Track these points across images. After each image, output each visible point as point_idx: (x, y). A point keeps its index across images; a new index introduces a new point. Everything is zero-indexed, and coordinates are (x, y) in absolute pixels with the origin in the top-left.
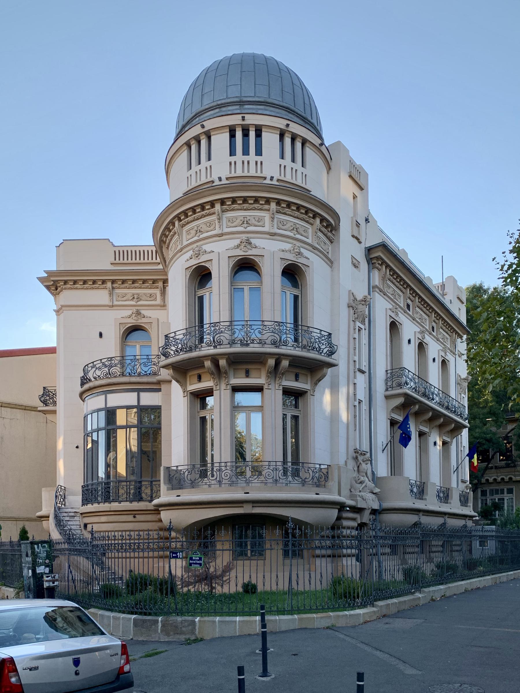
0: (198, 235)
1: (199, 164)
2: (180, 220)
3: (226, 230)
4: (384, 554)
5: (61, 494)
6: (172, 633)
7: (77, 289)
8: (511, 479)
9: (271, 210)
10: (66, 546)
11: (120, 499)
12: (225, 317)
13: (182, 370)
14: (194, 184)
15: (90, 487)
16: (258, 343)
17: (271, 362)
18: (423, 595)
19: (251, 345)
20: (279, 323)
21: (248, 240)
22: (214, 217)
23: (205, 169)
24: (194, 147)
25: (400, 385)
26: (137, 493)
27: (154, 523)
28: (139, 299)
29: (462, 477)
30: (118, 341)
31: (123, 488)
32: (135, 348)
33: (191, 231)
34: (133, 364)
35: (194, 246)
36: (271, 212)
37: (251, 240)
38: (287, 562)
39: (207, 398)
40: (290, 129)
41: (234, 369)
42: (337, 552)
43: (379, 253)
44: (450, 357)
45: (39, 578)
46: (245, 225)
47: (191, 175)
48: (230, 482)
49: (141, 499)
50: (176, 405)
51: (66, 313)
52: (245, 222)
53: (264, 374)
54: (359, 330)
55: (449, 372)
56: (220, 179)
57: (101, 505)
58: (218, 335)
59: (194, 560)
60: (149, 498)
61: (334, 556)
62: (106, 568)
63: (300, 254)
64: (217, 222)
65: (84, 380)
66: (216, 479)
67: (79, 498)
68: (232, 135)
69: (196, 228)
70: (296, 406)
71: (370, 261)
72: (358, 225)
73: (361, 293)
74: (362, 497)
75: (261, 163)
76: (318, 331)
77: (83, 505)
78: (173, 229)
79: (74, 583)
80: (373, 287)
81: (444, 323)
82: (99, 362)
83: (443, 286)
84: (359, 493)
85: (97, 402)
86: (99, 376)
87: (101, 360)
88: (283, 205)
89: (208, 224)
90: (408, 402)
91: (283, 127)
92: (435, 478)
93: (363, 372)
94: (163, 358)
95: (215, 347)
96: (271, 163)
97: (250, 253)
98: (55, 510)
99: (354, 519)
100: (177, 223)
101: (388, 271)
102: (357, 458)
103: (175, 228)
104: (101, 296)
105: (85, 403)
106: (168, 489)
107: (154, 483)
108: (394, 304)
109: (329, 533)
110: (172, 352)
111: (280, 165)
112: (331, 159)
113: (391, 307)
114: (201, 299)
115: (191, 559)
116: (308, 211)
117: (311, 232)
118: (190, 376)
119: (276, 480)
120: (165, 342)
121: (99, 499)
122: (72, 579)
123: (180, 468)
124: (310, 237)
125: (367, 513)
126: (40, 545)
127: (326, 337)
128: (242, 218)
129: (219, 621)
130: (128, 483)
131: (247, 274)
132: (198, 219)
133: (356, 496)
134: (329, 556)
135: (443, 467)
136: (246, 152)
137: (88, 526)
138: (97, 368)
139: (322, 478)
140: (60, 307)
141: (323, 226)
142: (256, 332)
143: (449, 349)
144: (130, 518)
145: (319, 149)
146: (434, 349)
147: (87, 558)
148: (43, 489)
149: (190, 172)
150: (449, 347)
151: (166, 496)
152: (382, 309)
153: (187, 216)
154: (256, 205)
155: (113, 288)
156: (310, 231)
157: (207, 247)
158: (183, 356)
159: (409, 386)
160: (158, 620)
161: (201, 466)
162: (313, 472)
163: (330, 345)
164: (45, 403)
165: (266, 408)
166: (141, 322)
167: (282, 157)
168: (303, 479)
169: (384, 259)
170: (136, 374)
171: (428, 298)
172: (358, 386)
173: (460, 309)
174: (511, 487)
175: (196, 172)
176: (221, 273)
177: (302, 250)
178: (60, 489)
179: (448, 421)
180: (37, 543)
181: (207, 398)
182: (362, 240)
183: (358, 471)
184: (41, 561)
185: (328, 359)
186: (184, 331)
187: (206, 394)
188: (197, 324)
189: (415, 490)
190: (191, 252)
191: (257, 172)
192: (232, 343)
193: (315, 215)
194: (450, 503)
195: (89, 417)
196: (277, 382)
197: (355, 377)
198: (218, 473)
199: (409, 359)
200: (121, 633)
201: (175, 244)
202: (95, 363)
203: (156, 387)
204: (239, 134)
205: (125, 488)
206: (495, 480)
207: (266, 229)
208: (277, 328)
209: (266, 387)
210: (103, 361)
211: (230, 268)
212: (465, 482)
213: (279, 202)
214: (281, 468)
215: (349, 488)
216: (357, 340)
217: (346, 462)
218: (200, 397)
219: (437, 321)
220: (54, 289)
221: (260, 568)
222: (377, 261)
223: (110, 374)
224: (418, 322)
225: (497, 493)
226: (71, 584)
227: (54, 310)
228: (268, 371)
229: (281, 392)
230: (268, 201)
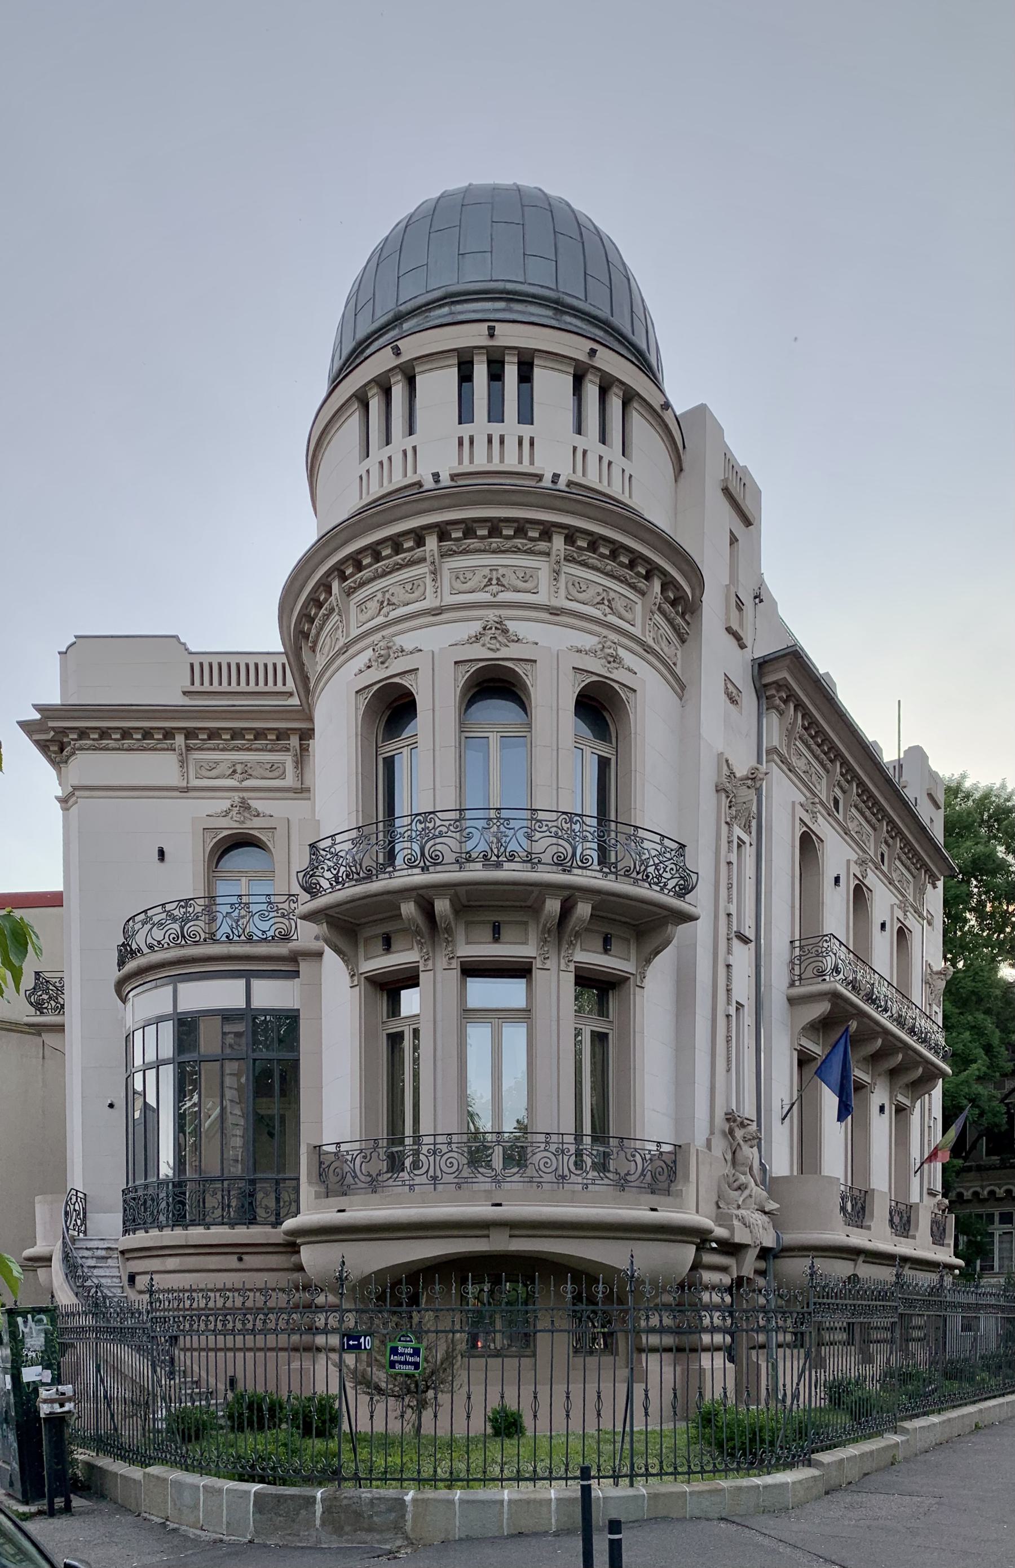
0: (385, 610)
1: (388, 442)
2: (344, 578)
3: (450, 599)
4: (831, 1344)
5: (77, 1208)
6: (347, 1529)
7: (108, 749)
9: (554, 552)
10: (88, 1321)
11: (208, 1219)
12: (448, 800)
13: (352, 926)
14: (376, 491)
15: (140, 1193)
16: (524, 862)
17: (553, 906)
18: (904, 1438)
19: (507, 865)
21: (500, 623)
22: (423, 569)
23: (401, 455)
24: (375, 404)
26: (246, 1205)
28: (247, 774)
29: (929, 1183)
30: (201, 868)
32: (242, 880)
33: (369, 604)
34: (236, 914)
35: (376, 637)
36: (553, 558)
37: (506, 622)
39: (402, 992)
40: (597, 362)
42: (687, 1340)
43: (782, 674)
44: (911, 922)
45: (28, 1395)
46: (495, 588)
47: (368, 471)
48: (456, 1180)
49: (252, 1221)
50: (333, 1007)
51: (83, 804)
52: (494, 582)
53: (533, 936)
54: (739, 846)
55: (907, 958)
57: (167, 1232)
58: (431, 843)
59: (402, 1354)
60: (273, 1219)
61: (680, 1350)
62: (179, 1371)
63: (616, 659)
64: (428, 580)
65: (126, 953)
66: (427, 1172)
67: (117, 1219)
68: (466, 377)
70: (602, 1010)
71: (761, 690)
72: (740, 605)
74: (742, 1220)
76: (657, 838)
77: (126, 1232)
78: (326, 600)
79: (109, 1406)
80: (768, 752)
81: (905, 845)
82: (159, 909)
84: (736, 1212)
85: (154, 1001)
86: (159, 942)
88: (580, 543)
89: (408, 587)
91: (583, 357)
94: (305, 896)
95: (425, 869)
96: (554, 442)
98: (64, 1244)
99: (724, 1269)
100: (335, 586)
102: (731, 1132)
103: (332, 598)
104: (160, 766)
105: (129, 1004)
106: (318, 1196)
108: (808, 795)
110: (325, 884)
111: (575, 449)
112: (684, 447)
113: (803, 799)
114: (389, 764)
115: (394, 1351)
116: (635, 559)
117: (640, 613)
118: (366, 940)
119: (563, 1177)
120: (311, 859)
121: (162, 1218)
122: (105, 1397)
123: (344, 1147)
124: (638, 622)
126: (29, 1316)
127: (673, 853)
128: (486, 571)
130: (226, 1183)
131: (497, 711)
132: (384, 574)
134: (668, 1350)
135: (896, 1156)
136: (496, 414)
137: (138, 1278)
138: (154, 925)
139: (666, 1173)
140: (71, 789)
142: (520, 834)
143: (912, 906)
144: (232, 1262)
146: (883, 902)
147: (139, 1349)
148: (38, 1198)
149: (368, 463)
151: (313, 1211)
152: (783, 800)
154: (519, 542)
155: (188, 749)
156: (638, 608)
157: (407, 641)
159: (841, 976)
160: (314, 1498)
161: (394, 1144)
162: (644, 1159)
164: (39, 1007)
165: (540, 1014)
166: (253, 825)
167: (579, 431)
168: (622, 1175)
170: (243, 938)
172: (735, 970)
174: (1006, 1209)
175: (381, 463)
176: (437, 700)
177: (622, 652)
178: (74, 1200)
179: (915, 1059)
180: (24, 1314)
181: (402, 992)
182: (748, 641)
183: (734, 1162)
186: (354, 834)
187: (398, 981)
188: (381, 818)
191: (520, 462)
192: (465, 859)
193: (652, 571)
195: (138, 1034)
196: (563, 954)
197: (729, 951)
198: (431, 1159)
199: (835, 915)
200: (224, 1527)
201: (330, 637)
203: (288, 966)
204: (480, 371)
205: (219, 1193)
206: (976, 1194)
207: (541, 598)
208: (565, 826)
209: (538, 964)
210: (168, 907)
211: (459, 690)
212: (935, 1195)
213: (571, 535)
215: (715, 1199)
217: (709, 1142)
219: (890, 841)
220: (56, 748)
221: (527, 1375)
222: (778, 691)
223: (183, 936)
226: (102, 1406)
227: (57, 798)
228: (545, 925)
229: (571, 977)
230: (547, 531)
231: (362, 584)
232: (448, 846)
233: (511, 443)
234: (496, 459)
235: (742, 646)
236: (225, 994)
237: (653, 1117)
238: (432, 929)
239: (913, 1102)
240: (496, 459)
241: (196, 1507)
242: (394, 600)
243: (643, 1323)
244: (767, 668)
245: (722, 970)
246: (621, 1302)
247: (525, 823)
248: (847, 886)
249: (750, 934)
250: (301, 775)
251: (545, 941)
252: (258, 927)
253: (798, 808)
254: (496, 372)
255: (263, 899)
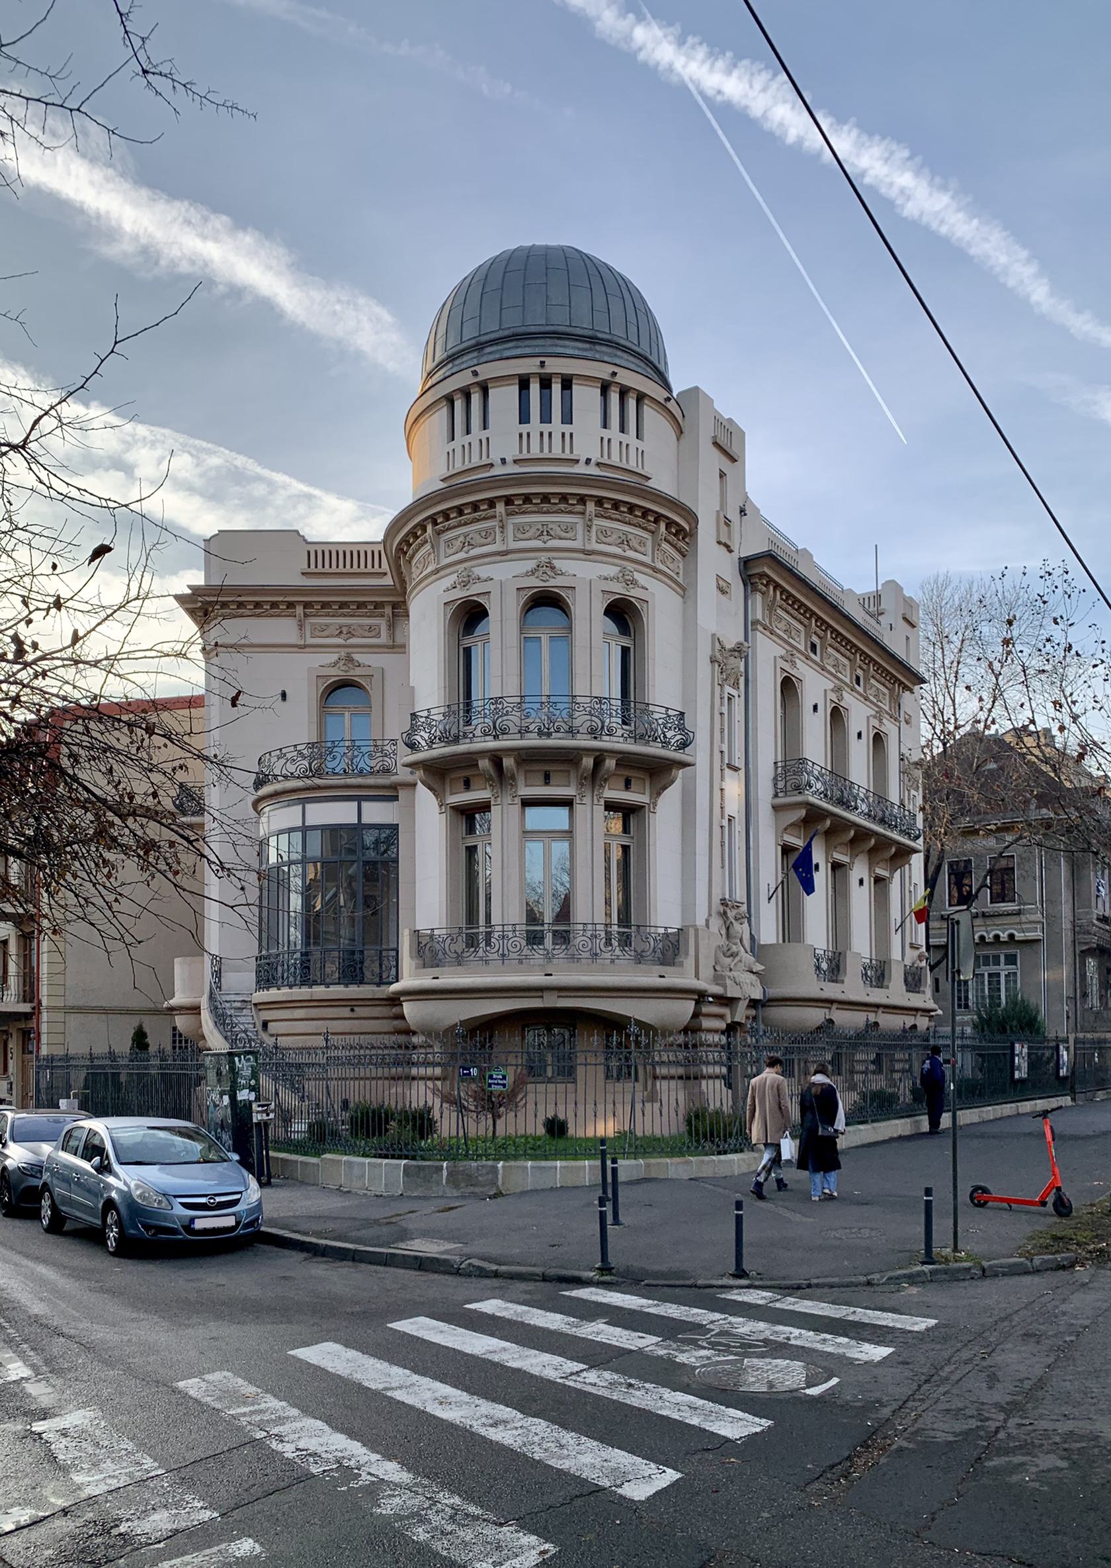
2: (435, 523)
6: (463, 1185)
8: (1011, 936)
12: (512, 689)
13: (440, 773)
17: (588, 762)
20: (600, 700)
24: (459, 404)
25: (798, 789)
27: (385, 1021)
31: (333, 963)
35: (461, 567)
37: (554, 562)
38: (610, 1087)
40: (617, 379)
41: (526, 772)
42: (693, 1070)
44: (889, 727)
49: (362, 982)
54: (729, 699)
56: (503, 461)
57: (295, 990)
60: (377, 980)
61: (688, 1078)
63: (634, 582)
67: (249, 978)
69: (462, 539)
72: (728, 522)
73: (733, 636)
75: (571, 435)
76: (663, 710)
83: (878, 597)
84: (729, 974)
87: (295, 746)
89: (483, 534)
90: (812, 817)
91: (607, 377)
92: (861, 945)
93: (736, 769)
95: (496, 737)
96: (587, 437)
97: (552, 583)
99: (721, 1017)
100: (429, 528)
101: (778, 593)
102: (725, 913)
104: (282, 629)
107: (384, 953)
109: (681, 1039)
114: (468, 652)
115: (491, 1077)
119: (596, 954)
123: (436, 932)
125: (743, 1005)
129: (532, 1167)
132: (466, 524)
133: (723, 977)
134: (680, 1078)
136: (546, 418)
139: (671, 949)
141: (670, 533)
144: (346, 1012)
145: (662, 406)
146: (859, 716)
150: (887, 708)
151: (410, 977)
153: (447, 518)
154: (562, 506)
155: (306, 615)
157: (482, 571)
158: (441, 750)
162: (655, 940)
163: (681, 728)
166: (354, 673)
169: (772, 576)
171: (848, 631)
172: (726, 793)
173: (908, 638)
174: (1012, 951)
177: (637, 575)
182: (735, 547)
184: (243, 1082)
185: (678, 756)
189: (824, 966)
190: (454, 577)
191: (563, 451)
192: (523, 732)
194: (887, 987)
197: (722, 779)
199: (815, 745)
202: (284, 751)
203: (390, 793)
204: (535, 387)
208: (597, 706)
210: (299, 748)
214: (603, 934)
216: (726, 716)
217: (707, 921)
218: (468, 816)
219: (865, 667)
221: (571, 1097)
224: (831, 674)
225: (986, 964)
231: (449, 529)
232: (513, 720)
233: (557, 438)
234: (546, 449)
235: (731, 551)
236: (342, 813)
237: (664, 912)
238: (501, 777)
239: (892, 873)
240: (546, 449)
241: (363, 1176)
242: (472, 542)
243: (657, 1059)
244: (750, 564)
245: (717, 793)
246: (626, 1047)
247: (567, 705)
248: (823, 715)
249: (739, 762)
250: (392, 635)
251: (582, 785)
252: (365, 763)
253: (780, 661)
254: (543, 392)
255: (372, 743)
